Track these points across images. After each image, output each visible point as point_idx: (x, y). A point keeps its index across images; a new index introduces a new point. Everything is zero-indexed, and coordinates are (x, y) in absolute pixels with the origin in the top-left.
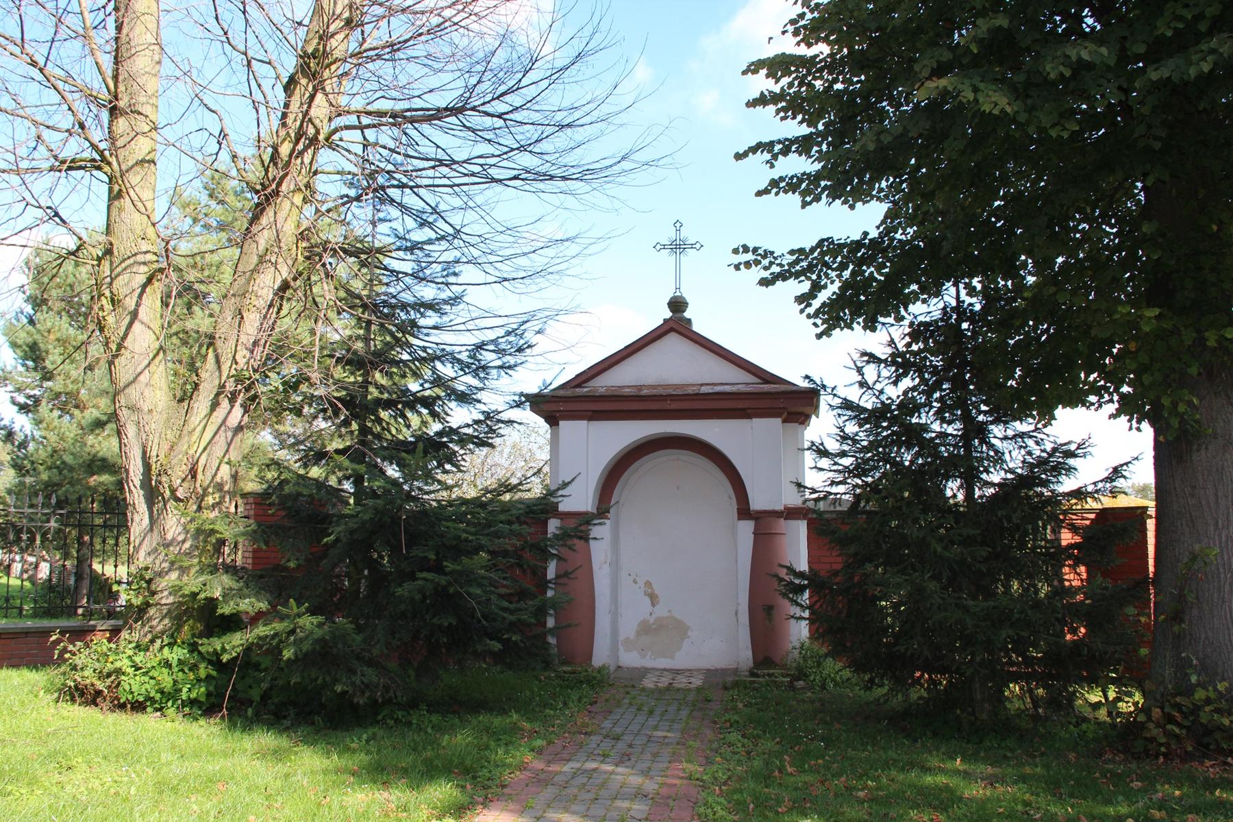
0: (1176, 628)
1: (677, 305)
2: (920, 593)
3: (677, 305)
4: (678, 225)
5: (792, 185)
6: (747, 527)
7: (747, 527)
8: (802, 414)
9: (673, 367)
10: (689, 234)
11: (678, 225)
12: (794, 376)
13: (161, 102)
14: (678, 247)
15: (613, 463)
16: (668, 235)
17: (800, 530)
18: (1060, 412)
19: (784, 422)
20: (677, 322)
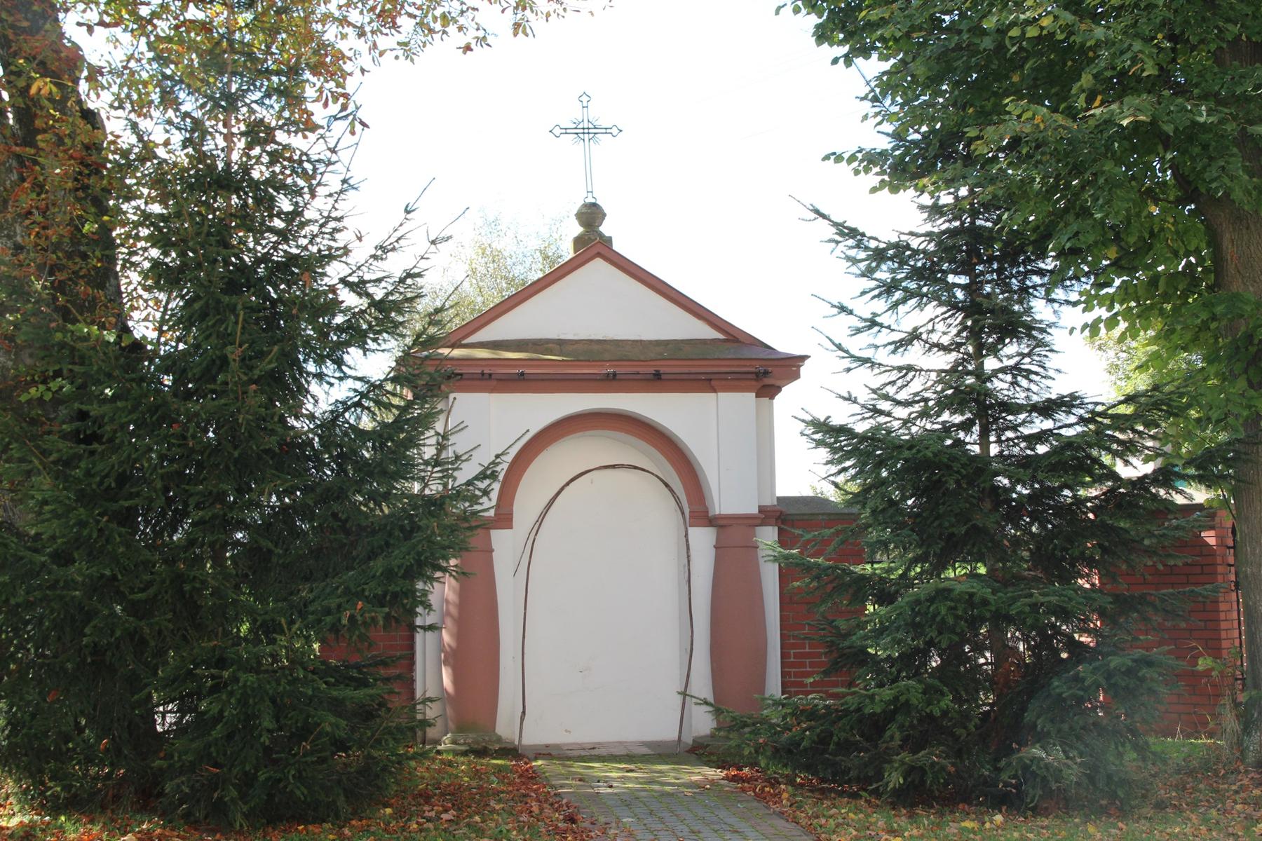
0: (961, 435)
1: (591, 215)
2: (928, 636)
3: (591, 215)
4: (585, 99)
5: (874, 297)
6: (702, 539)
7: (702, 539)
8: (772, 386)
9: (592, 311)
10: (600, 114)
11: (585, 99)
12: (784, 344)
13: (560, 253)
14: (586, 131)
15: (681, 446)
16: (570, 114)
17: (768, 536)
18: (755, 511)
19: (757, 396)
20: (593, 244)
